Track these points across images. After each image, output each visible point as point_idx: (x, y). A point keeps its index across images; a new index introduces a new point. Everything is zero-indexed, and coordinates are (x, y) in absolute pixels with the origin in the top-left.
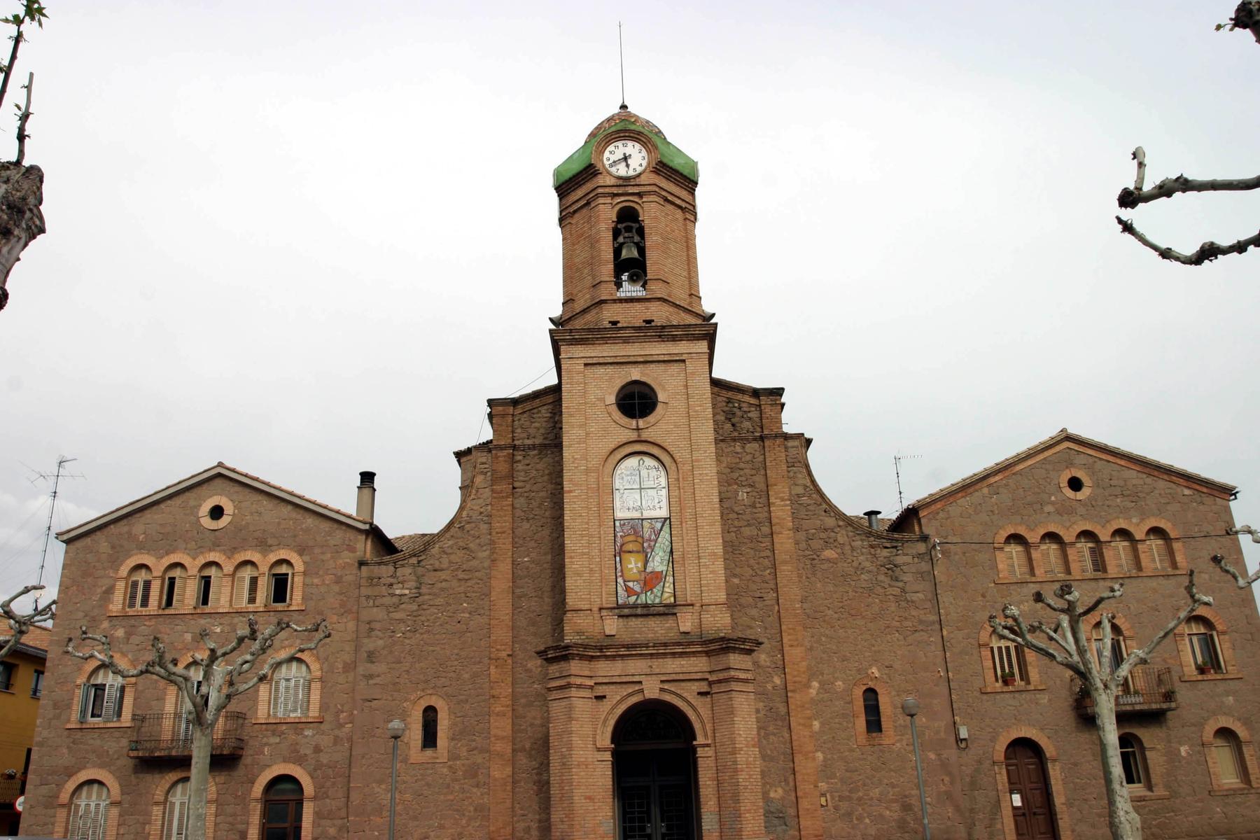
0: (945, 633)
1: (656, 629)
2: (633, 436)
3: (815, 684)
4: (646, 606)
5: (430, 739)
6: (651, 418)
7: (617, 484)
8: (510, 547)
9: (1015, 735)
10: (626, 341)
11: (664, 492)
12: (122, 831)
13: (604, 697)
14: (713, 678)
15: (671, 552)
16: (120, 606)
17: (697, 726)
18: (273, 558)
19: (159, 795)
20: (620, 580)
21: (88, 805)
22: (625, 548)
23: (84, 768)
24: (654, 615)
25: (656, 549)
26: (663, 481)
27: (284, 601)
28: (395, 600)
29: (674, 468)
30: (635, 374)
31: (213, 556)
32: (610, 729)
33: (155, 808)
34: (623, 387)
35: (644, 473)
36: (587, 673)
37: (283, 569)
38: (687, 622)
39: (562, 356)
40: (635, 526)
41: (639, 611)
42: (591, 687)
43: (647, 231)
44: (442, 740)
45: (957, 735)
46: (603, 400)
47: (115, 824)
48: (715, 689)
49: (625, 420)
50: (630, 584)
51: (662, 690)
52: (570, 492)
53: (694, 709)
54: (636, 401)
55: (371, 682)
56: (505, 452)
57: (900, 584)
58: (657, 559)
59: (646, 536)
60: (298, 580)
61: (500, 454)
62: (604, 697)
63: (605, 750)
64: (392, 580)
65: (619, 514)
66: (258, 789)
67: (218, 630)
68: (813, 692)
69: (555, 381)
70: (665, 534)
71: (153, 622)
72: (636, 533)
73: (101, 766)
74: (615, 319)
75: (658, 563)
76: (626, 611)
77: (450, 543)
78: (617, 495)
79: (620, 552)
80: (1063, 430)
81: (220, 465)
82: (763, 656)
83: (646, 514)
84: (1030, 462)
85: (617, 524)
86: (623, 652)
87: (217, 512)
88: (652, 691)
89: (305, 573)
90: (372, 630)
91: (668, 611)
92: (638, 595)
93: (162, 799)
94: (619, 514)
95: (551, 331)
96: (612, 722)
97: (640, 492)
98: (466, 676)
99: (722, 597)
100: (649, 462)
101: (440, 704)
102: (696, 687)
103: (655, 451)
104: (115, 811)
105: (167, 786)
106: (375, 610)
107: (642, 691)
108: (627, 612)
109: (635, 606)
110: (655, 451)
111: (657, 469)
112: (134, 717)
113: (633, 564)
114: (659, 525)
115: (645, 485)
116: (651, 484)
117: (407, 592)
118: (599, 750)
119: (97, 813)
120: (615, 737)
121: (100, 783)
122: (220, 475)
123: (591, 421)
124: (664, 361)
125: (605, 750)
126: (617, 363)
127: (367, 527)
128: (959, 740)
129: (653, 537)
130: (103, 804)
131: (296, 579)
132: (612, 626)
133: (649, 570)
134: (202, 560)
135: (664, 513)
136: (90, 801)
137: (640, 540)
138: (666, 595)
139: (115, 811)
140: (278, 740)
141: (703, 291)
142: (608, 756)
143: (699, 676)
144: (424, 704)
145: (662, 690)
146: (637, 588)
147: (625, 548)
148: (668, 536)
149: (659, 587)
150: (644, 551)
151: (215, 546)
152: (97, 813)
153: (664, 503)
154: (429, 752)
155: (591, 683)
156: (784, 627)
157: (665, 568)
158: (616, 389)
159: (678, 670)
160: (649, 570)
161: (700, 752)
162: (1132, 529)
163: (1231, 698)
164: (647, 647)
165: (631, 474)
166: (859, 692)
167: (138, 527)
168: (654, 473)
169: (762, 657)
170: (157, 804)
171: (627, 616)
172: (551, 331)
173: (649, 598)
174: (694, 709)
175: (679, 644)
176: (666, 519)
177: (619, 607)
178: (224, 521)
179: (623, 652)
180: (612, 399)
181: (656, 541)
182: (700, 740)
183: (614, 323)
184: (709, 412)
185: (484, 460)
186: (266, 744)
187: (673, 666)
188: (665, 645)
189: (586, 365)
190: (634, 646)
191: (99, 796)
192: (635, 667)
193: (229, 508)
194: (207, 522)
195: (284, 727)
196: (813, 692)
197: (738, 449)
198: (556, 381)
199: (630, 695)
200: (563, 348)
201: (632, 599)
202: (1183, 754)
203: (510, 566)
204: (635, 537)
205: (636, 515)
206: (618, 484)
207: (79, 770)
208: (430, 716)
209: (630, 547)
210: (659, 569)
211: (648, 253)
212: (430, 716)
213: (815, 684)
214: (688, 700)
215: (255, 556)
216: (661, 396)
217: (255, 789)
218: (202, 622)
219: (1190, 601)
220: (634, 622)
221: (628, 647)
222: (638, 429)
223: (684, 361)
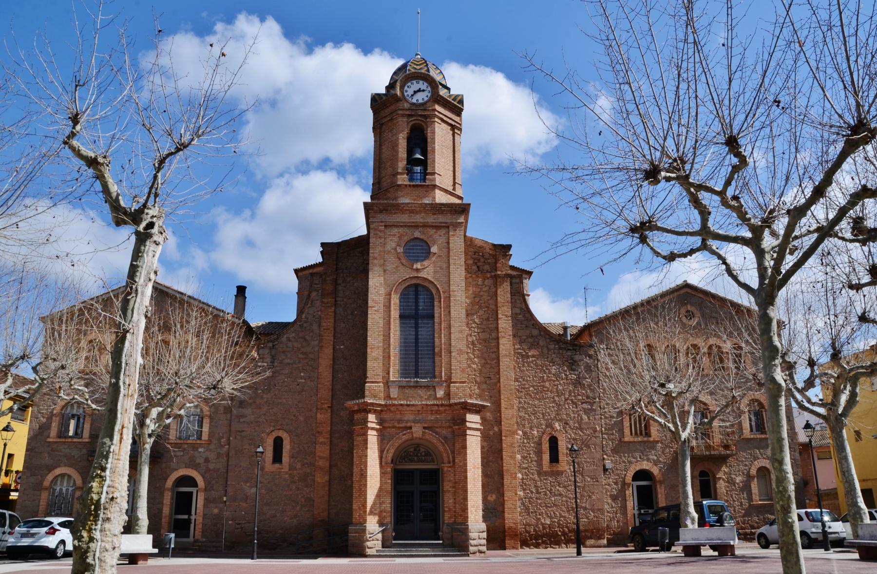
5: (277, 457)
21: (61, 490)
44: (286, 459)
55: (242, 420)
66: (169, 483)
95: (365, 204)
101: (285, 436)
121: (69, 477)
130: (71, 489)
144: (275, 434)
154: (277, 465)
185: (317, 282)
203: (332, 351)
208: (278, 443)
212: (278, 443)
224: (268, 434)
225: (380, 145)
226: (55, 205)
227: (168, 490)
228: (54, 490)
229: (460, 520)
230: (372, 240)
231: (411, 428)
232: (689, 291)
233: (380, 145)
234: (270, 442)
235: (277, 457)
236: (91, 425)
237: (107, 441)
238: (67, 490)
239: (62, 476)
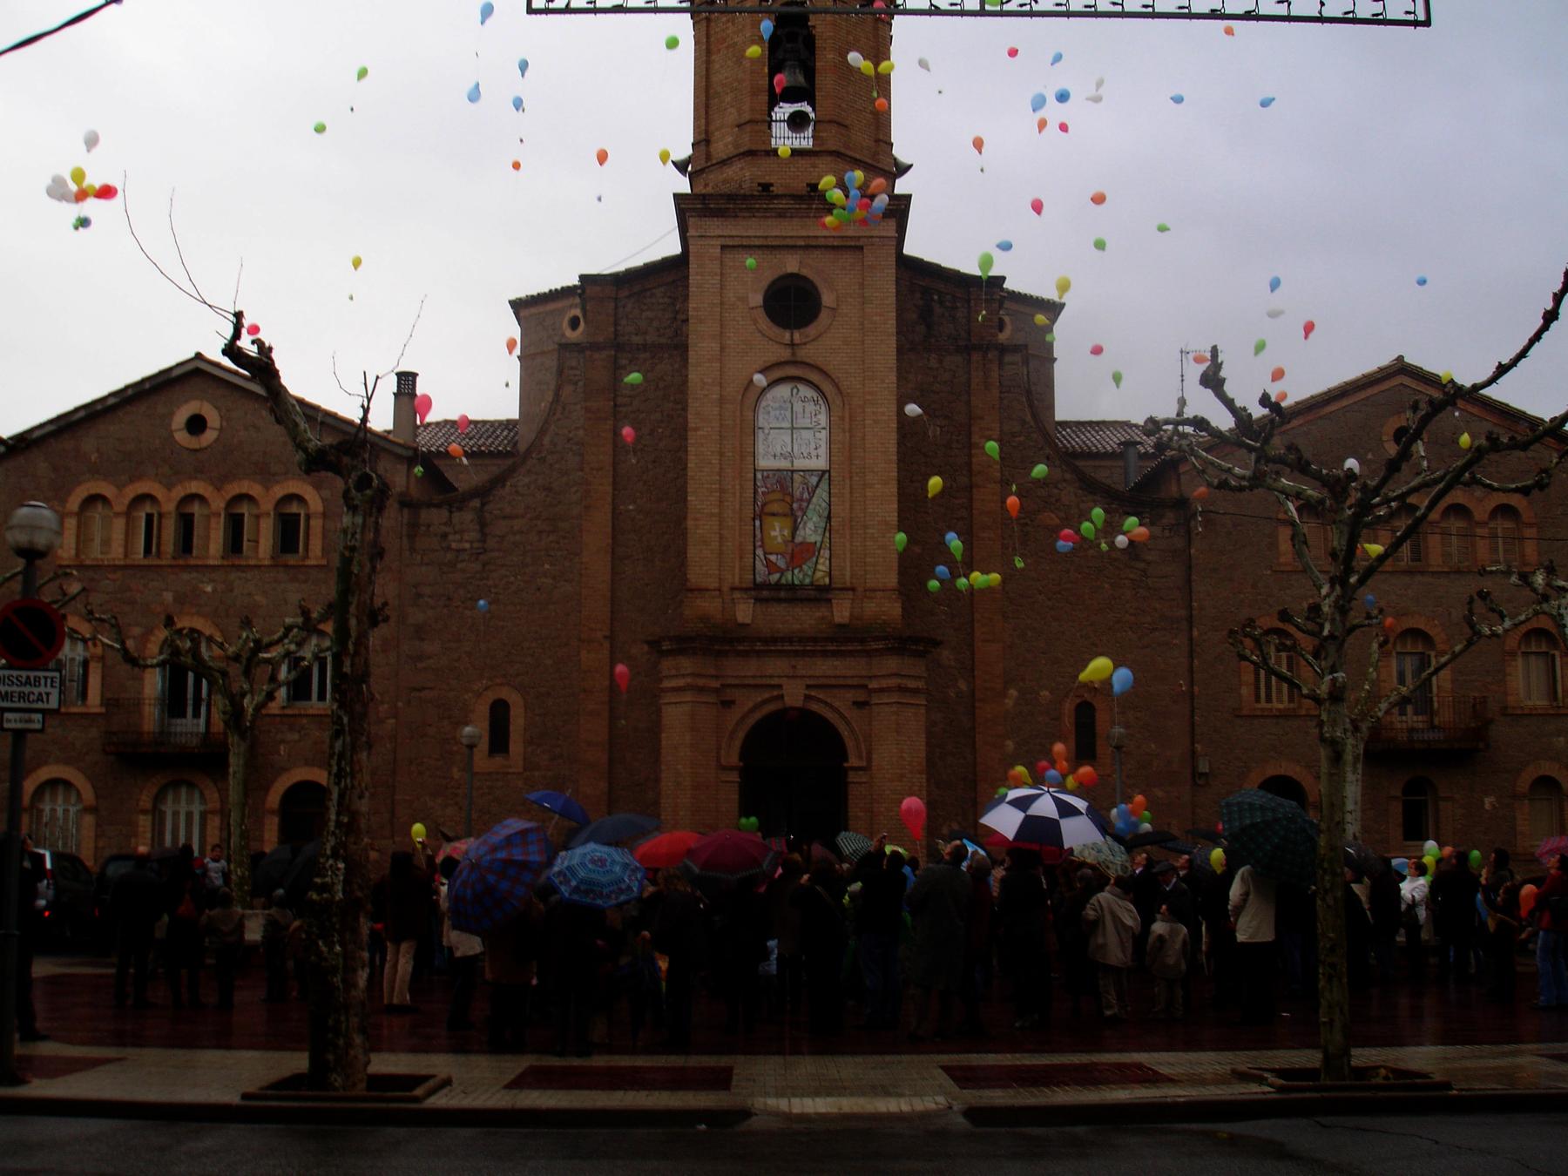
0: (1195, 633)
1: (804, 619)
2: (785, 354)
3: (1013, 692)
4: (791, 587)
5: (499, 740)
6: (812, 330)
7: (761, 422)
8: (610, 489)
9: (1271, 771)
10: (781, 215)
11: (824, 435)
12: (101, 844)
13: (733, 702)
14: (873, 685)
15: (829, 518)
16: (73, 552)
17: (850, 744)
18: (279, 491)
19: (146, 801)
20: (759, 552)
21: (53, 811)
22: (768, 509)
23: (46, 763)
24: (802, 600)
25: (810, 513)
26: (823, 419)
27: (297, 551)
28: (449, 556)
29: (839, 402)
30: (791, 264)
31: (195, 487)
32: (737, 744)
33: (141, 817)
34: (774, 283)
35: (798, 407)
36: (712, 671)
37: (294, 508)
38: (841, 612)
39: (691, 232)
40: (783, 479)
41: (783, 594)
42: (716, 691)
43: (818, 43)
44: (516, 746)
45: (1194, 767)
46: (744, 299)
47: (92, 834)
48: (875, 700)
49: (775, 331)
50: (773, 558)
51: (808, 697)
52: (696, 429)
53: (848, 723)
54: (792, 303)
55: (419, 665)
56: (604, 354)
57: (1142, 565)
58: (810, 525)
59: (797, 494)
60: (316, 524)
61: (596, 356)
62: (733, 702)
63: (731, 768)
64: (447, 529)
65: (764, 463)
66: (274, 798)
67: (209, 589)
68: (1009, 702)
69: (676, 249)
70: (824, 485)
71: (119, 574)
72: (783, 489)
73: (67, 762)
74: (767, 179)
75: (810, 531)
76: (765, 593)
77: (527, 480)
78: (760, 435)
79: (761, 514)
80: (1400, 358)
81: (199, 356)
82: (946, 653)
83: (800, 464)
84: (1345, 402)
85: (759, 476)
86: (759, 646)
87: (196, 424)
88: (794, 695)
89: (324, 515)
90: (419, 595)
91: (821, 594)
92: (782, 572)
93: (149, 805)
94: (764, 463)
95: (678, 198)
96: (741, 735)
97: (793, 435)
98: (549, 662)
99: (892, 580)
100: (806, 391)
101: (514, 698)
102: (850, 695)
103: (814, 377)
104: (89, 820)
105: (155, 790)
106: (424, 569)
107: (782, 697)
108: (767, 593)
109: (778, 586)
110: (814, 377)
111: (816, 403)
112: (106, 702)
113: (777, 531)
114: (814, 480)
115: (800, 422)
116: (806, 422)
117: (467, 546)
118: (724, 768)
119: (66, 819)
120: (743, 755)
121: (67, 784)
122: (197, 372)
123: (728, 326)
124: (834, 248)
125: (731, 768)
126: (767, 247)
127: (410, 453)
128: (1196, 775)
129: (806, 495)
130: (72, 810)
131: (313, 522)
132: (744, 612)
133: (798, 539)
134: (179, 492)
135: (821, 463)
136: (57, 808)
137: (788, 499)
138: (819, 574)
139: (89, 820)
140: (296, 736)
141: (896, 136)
142: (734, 777)
143: (855, 682)
144: (491, 696)
145: (808, 697)
146: (782, 564)
147: (768, 509)
148: (825, 495)
149: (811, 563)
150: (792, 513)
151: (198, 472)
152: (66, 819)
153: (823, 451)
154: (499, 760)
155: (716, 684)
156: (977, 616)
157: (819, 539)
158: (765, 284)
159: (829, 673)
160: (798, 539)
161: (852, 777)
162: (1471, 506)
163: (1562, 739)
164: (790, 640)
165: (781, 408)
166: (1069, 707)
167: (89, 443)
168: (811, 407)
169: (946, 654)
170: (144, 812)
171: (767, 600)
172: (678, 198)
173: (796, 576)
174: (848, 723)
175: (831, 640)
176: (824, 472)
177: (757, 587)
178: (209, 436)
179: (759, 646)
180: (757, 299)
181: (809, 502)
182: (853, 761)
183: (766, 187)
184: (891, 325)
185: (574, 364)
186: (283, 741)
187: (824, 668)
188: (815, 640)
189: (723, 247)
190: (774, 640)
191: (67, 800)
192: (775, 667)
193: (213, 417)
194: (182, 437)
195: (305, 721)
196: (1009, 702)
197: (933, 363)
198: (676, 249)
199: (765, 702)
200: (692, 221)
201: (775, 577)
202: (1487, 806)
203: (609, 516)
204: (783, 494)
205: (784, 464)
206: (762, 421)
207: (39, 766)
208: (499, 713)
209: (775, 508)
210: (812, 539)
211: (819, 79)
212: (499, 713)
213: (1013, 692)
214: (838, 709)
215: (255, 490)
216: (827, 299)
217: (270, 798)
218: (185, 576)
219: (1467, 630)
220: (778, 610)
221: (766, 641)
222: (792, 345)
223: (861, 248)
224: (479, 695)
225: (708, 62)
226: (275, 566)
227: (272, 812)
228: (41, 811)
229: (1012, 783)
230: (693, 266)
231: (780, 686)
232: (1407, 381)
233: (709, 52)
234: (482, 710)
235: (499, 740)
236: (103, 678)
237: (755, 1123)
238: (66, 811)
239: (53, 783)
